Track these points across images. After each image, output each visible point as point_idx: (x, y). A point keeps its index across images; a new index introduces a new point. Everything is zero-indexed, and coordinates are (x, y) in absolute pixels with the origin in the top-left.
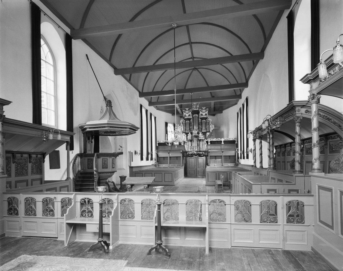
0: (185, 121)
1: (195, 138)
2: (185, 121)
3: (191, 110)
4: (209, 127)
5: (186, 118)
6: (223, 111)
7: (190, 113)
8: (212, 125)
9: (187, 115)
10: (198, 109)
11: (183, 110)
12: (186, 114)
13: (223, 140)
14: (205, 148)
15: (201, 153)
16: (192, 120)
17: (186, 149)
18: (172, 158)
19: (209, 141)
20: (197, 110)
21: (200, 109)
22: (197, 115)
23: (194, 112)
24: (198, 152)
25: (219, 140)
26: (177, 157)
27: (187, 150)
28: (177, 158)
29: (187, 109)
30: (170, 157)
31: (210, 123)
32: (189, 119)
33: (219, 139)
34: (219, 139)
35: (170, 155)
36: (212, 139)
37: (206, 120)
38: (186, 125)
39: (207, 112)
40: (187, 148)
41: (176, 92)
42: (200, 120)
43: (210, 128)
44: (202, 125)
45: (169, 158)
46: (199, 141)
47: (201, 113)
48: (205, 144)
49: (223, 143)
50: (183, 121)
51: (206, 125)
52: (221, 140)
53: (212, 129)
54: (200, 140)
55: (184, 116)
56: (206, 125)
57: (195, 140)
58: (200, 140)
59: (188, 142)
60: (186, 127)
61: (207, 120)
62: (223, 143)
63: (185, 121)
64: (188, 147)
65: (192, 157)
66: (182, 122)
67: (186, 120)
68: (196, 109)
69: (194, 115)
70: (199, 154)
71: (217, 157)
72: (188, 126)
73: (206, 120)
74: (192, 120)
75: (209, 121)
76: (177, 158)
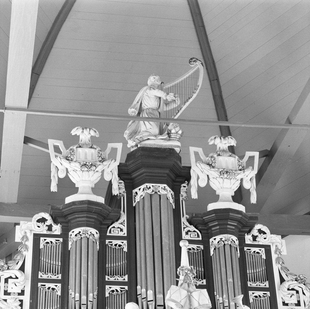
0: (65, 235)
2: (57, 229)
3: (119, 146)
8: (295, 285)
9: (225, 188)
10: (175, 144)
11: (51, 142)
12: (213, 173)
20: (170, 152)
21: (192, 149)
22: (165, 190)
23: (144, 165)
29: (85, 135)
32: (100, 215)
38: (65, 269)
39: (252, 173)
47: (200, 175)
50: (43, 230)
55: (54, 188)
63: (65, 235)
66: (37, 237)
67: (66, 217)
68: (160, 142)
69: (140, 193)
72: (83, 272)
74: (119, 228)
75: (267, 248)
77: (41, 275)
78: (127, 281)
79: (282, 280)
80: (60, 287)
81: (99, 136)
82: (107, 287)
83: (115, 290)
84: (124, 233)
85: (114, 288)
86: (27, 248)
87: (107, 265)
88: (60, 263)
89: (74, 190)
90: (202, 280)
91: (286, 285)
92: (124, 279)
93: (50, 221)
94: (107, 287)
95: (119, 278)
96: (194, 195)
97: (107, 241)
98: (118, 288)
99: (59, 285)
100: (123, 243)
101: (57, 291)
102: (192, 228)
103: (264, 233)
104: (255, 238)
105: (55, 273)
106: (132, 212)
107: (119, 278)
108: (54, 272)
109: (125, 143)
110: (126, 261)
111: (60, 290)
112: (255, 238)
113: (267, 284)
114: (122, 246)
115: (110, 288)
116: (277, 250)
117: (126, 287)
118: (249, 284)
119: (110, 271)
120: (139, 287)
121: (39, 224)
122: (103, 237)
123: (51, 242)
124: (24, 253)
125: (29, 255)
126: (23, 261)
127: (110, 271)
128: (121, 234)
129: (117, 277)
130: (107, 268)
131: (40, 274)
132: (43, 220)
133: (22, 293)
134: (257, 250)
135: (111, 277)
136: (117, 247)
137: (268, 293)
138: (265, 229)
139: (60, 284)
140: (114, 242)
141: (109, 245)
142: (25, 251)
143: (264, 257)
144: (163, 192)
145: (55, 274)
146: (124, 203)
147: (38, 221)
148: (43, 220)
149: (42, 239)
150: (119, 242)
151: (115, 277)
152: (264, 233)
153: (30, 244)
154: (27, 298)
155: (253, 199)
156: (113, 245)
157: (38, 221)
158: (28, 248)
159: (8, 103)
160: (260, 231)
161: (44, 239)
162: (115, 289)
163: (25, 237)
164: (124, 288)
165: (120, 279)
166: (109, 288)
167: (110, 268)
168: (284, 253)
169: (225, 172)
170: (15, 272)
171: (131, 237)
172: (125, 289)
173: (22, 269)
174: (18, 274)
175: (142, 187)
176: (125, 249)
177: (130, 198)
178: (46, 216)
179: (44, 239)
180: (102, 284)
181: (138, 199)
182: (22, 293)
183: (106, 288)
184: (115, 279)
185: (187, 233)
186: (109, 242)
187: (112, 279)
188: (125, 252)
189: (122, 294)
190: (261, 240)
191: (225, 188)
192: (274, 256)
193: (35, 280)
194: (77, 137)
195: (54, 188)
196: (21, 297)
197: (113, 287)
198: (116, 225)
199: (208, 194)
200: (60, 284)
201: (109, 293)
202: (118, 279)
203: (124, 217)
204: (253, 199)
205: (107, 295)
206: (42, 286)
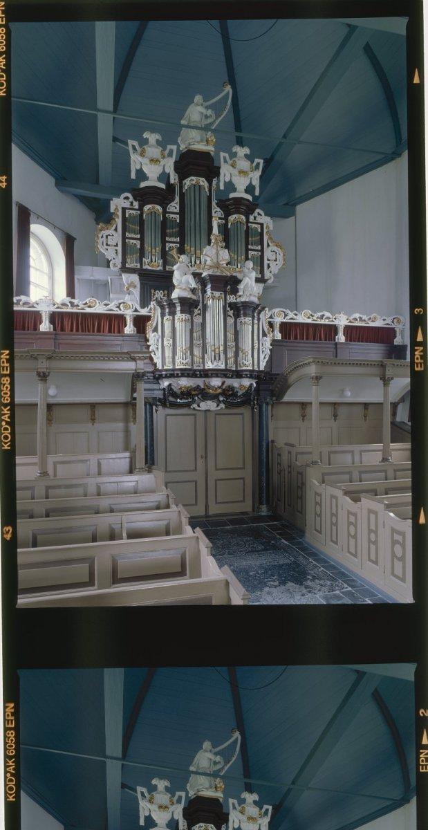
0: (141, 208)
1: (217, 294)
2: (136, 205)
4: (262, 257)
5: (143, 185)
6: (299, 208)
7: (169, 165)
8: (275, 249)
13: (342, 321)
14: (262, 357)
15: (246, 382)
16: (174, 206)
17: (158, 360)
18: (56, 412)
19: (278, 320)
22: (203, 182)
23: (196, 164)
24: (229, 382)
25: (327, 322)
26: (93, 406)
27: (159, 366)
28: (93, 414)
30: (50, 407)
31: (266, 238)
32: (162, 196)
33: (327, 314)
34: (326, 318)
35: (52, 392)
36: (291, 315)
37: (247, 219)
39: (258, 174)
40: (159, 353)
41: (406, 350)
42: (217, 212)
43: (266, 262)
44: (142, 232)
45: (41, 412)
46: (237, 316)
47: (226, 173)
48: (264, 335)
49: (341, 338)
50: (127, 205)
51: (247, 243)
52: (336, 322)
53: (275, 268)
54: (238, 310)
55: (133, 176)
56: (247, 243)
57: (214, 303)
58: (238, 310)
59: (173, 313)
60: (142, 240)
61: (251, 218)
62: (341, 338)
63: (141, 208)
64: (168, 342)
65: (188, 405)
66: (124, 209)
67: (145, 196)
69: (187, 182)
70: (231, 388)
71: (99, 412)
73: (247, 219)
74: (174, 206)
75: (262, 225)
76: (93, 414)
77: (250, 247)
79: (268, 245)
81: (153, 291)
82: (167, 244)
84: (177, 210)
85: (253, 253)
86: (118, 216)
89: (145, 178)
91: (270, 248)
93: (131, 199)
94: (167, 244)
96: (222, 187)
98: (256, 253)
102: (218, 209)
103: (261, 215)
104: (255, 218)
106: (182, 196)
108: (136, 233)
109: (179, 146)
112: (255, 218)
113: (259, 247)
116: (267, 226)
117: (178, 245)
118: (167, 239)
120: (186, 245)
121: (125, 201)
122: (165, 212)
125: (119, 221)
128: (175, 211)
131: (127, 234)
132: (127, 198)
133: (117, 245)
134: (256, 226)
137: (260, 253)
138: (262, 212)
140: (132, 241)
143: (259, 230)
144: (201, 183)
146: (177, 189)
147: (125, 198)
148: (127, 198)
149: (127, 211)
150: (134, 242)
152: (261, 215)
153: (120, 213)
154: (120, 248)
155: (257, 193)
157: (125, 198)
159: (108, 753)
160: (259, 214)
163: (116, 209)
168: (271, 228)
169: (242, 172)
170: (111, 231)
171: (182, 213)
173: (116, 230)
174: (114, 233)
175: (189, 179)
176: (178, 221)
177: (181, 187)
178: (129, 195)
180: (164, 242)
181: (186, 187)
182: (117, 245)
185: (215, 213)
187: (170, 240)
190: (259, 220)
191: (241, 183)
192: (265, 231)
193: (124, 238)
194: (147, 140)
195: (133, 176)
196: (116, 248)
198: (172, 204)
199: (230, 186)
203: (177, 199)
204: (257, 193)
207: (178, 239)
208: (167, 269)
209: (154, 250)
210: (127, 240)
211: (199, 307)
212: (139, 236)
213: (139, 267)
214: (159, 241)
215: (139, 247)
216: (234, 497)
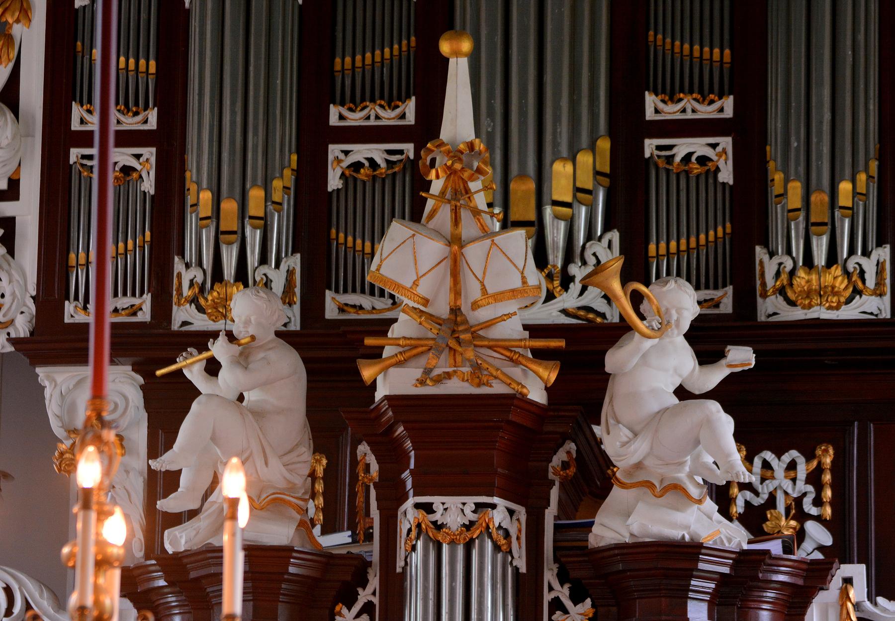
41: (414, 486)
44: (171, 95)
60: (169, 143)
78: (413, 122)
80: (153, 160)
82: (334, 150)
83: (367, 164)
85: (361, 152)
87: (338, 60)
88: (152, 63)
90: (720, 98)
92: (403, 116)
94: (334, 150)
95: (381, 113)
97: (650, 146)
98: (376, 151)
99: (149, 153)
100: (714, 146)
101: (141, 177)
105: (136, 104)
107: (381, 113)
108: (131, 103)
110: (728, 225)
111: (153, 173)
114: (710, 160)
115: (346, 153)
119: (348, 82)
123: (371, 161)
124: (17, 30)
126: (11, 65)
127: (348, 82)
129: (374, 109)
130: (336, 74)
135: (351, 110)
136: (696, 169)
139: (154, 150)
140: (683, 146)
141: (662, 164)
142: (18, 21)
145: (134, 109)
150: (698, 146)
151: (368, 109)
156: (678, 159)
158: (30, 8)
161: (342, 151)
162: (367, 159)
164: (401, 152)
165: (388, 117)
166: (342, 156)
167: (350, 72)
172: (403, 157)
176: (726, 175)
179: (342, 151)
183: (331, 157)
184: (368, 118)
186: (659, 148)
187: (355, 119)
188: (724, 184)
189: (394, 174)
193: (58, 137)
197: (358, 151)
200: (154, 150)
201: (343, 175)
202: (377, 117)
205: (334, 182)
206: (85, 162)
207: (153, 116)
208: (331, 312)
209: (229, 206)
210: (650, 146)
211: (364, 596)
212: (152, 119)
213: (145, 316)
214: (286, 130)
215: (149, 185)
216: (689, 387)
